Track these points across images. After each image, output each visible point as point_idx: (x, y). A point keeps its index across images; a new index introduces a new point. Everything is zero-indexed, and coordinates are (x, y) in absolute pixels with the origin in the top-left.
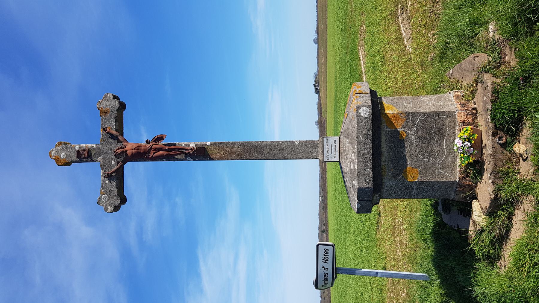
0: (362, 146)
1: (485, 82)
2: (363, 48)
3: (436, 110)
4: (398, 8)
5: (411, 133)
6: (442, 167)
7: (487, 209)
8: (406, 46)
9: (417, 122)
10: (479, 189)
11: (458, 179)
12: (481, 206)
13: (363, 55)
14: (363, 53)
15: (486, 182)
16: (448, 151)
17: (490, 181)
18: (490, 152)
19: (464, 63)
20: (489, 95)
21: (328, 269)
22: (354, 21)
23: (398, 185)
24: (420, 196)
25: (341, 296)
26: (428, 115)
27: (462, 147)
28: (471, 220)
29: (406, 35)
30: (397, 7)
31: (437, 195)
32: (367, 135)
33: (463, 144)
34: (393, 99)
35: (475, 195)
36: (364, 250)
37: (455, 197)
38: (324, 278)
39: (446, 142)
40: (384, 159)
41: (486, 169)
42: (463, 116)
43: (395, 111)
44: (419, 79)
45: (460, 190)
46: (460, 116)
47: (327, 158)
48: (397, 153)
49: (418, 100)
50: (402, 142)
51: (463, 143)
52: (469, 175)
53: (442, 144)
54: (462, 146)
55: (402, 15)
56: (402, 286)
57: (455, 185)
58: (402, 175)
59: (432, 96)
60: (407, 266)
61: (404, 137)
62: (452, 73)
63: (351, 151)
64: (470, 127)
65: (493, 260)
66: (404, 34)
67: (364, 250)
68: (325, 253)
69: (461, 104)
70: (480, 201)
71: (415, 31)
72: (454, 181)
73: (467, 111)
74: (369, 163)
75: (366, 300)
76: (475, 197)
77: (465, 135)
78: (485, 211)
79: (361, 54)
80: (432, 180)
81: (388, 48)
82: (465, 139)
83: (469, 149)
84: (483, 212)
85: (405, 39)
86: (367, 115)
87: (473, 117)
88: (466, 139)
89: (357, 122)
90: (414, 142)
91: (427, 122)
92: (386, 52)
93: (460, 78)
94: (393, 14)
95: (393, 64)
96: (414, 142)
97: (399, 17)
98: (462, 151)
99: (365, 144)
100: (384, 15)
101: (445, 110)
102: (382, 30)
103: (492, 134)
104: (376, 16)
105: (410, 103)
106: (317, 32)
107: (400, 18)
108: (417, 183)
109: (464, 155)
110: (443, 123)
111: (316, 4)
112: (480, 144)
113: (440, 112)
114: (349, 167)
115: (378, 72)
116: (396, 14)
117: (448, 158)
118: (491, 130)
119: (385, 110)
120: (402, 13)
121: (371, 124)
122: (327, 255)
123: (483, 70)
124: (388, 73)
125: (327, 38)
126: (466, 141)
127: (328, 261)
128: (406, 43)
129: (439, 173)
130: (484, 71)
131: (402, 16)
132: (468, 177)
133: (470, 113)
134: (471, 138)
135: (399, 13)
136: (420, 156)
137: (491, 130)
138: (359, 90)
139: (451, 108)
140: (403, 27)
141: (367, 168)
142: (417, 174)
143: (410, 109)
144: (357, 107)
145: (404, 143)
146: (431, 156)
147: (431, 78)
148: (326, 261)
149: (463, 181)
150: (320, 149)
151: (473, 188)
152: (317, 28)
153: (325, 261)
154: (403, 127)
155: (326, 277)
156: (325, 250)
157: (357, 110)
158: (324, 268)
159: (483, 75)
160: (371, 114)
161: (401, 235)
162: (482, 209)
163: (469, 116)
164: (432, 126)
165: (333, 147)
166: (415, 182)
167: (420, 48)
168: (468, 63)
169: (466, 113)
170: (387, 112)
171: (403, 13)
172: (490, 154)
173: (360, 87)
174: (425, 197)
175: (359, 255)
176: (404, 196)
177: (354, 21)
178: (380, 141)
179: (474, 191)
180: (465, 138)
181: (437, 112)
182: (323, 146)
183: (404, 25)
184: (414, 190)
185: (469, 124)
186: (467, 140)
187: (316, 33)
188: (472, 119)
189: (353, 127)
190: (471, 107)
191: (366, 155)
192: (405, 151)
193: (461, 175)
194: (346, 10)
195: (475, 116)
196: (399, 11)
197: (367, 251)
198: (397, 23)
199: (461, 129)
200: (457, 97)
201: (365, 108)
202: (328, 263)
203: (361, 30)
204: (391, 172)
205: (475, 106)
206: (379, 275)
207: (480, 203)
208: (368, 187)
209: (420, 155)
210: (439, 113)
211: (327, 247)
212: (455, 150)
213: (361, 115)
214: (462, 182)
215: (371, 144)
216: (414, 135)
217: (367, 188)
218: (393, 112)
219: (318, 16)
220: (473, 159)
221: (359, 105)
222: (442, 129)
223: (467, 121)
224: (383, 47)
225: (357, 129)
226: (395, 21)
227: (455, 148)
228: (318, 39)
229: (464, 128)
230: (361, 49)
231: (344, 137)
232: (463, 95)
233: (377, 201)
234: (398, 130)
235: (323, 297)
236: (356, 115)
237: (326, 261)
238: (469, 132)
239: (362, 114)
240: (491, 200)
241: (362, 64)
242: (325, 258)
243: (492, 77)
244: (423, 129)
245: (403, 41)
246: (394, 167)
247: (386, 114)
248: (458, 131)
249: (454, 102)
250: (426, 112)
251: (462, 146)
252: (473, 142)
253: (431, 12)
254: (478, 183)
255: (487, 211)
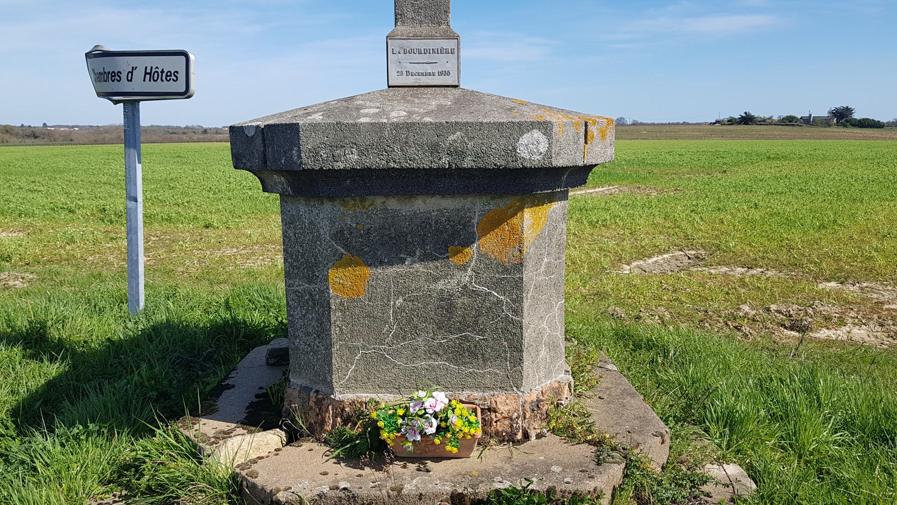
0: (430, 137)
1: (601, 469)
2: (617, 192)
3: (526, 342)
4: (700, 249)
5: (466, 277)
6: (371, 357)
7: (249, 478)
8: (628, 265)
9: (496, 294)
10: (311, 450)
11: (338, 396)
12: (262, 458)
13: (603, 192)
14: (606, 192)
15: (325, 474)
16: (414, 372)
17: (326, 489)
18: (409, 488)
19: (637, 403)
20: (568, 483)
21: (131, 80)
22: (661, 177)
23: (319, 243)
24: (293, 300)
25: (179, 156)
26: (512, 322)
27: (424, 411)
28: (233, 425)
29: (649, 264)
30: (701, 248)
31: (296, 344)
32: (462, 154)
33: (431, 415)
34: (560, 230)
35: (297, 439)
36: (250, 193)
37: (293, 385)
38: (109, 73)
39: (438, 366)
40: (393, 204)
41: (360, 476)
42: (507, 408)
43: (529, 235)
44: (570, 289)
45: (311, 402)
46: (507, 401)
47: (396, 50)
48: (409, 239)
49: (554, 295)
50: (441, 254)
51: (435, 415)
52: (350, 424)
53: (433, 356)
54: (426, 413)
55: (687, 257)
56: (162, 257)
57: (322, 388)
58: (345, 252)
59: (562, 328)
60: (198, 265)
61: (454, 260)
62: (607, 370)
63: (413, 109)
64: (479, 434)
65: (125, 482)
66: (650, 261)
67: (250, 193)
68: (169, 74)
69: (539, 401)
70: (277, 455)
71: (663, 281)
72: (333, 388)
73: (520, 419)
74: (378, 160)
75: (158, 195)
76: (293, 437)
77: (454, 420)
78: (246, 471)
79: (605, 188)
80: (334, 332)
81: (622, 233)
82: (446, 419)
83: (417, 432)
84: (242, 467)
85: (642, 262)
86: (523, 152)
87: (504, 434)
88: (446, 422)
89: (502, 124)
90: (440, 285)
91: (493, 320)
92: (615, 230)
93: (600, 391)
94: (689, 241)
95: (595, 240)
96: (440, 285)
97: (682, 251)
98: (411, 410)
99: (434, 149)
100: (684, 224)
101: (526, 363)
102: (655, 222)
103: (459, 494)
104: (679, 211)
105: (546, 273)
106: (635, 124)
107: (681, 253)
108: (324, 292)
109: (400, 416)
110: (490, 359)
111: (681, 122)
112: (430, 455)
113: (522, 351)
114: (368, 103)
115: (577, 215)
116: (687, 246)
117: (395, 371)
118: (470, 490)
119: (531, 207)
120: (690, 256)
121: (495, 165)
122: (164, 78)
123: (632, 461)
124: (576, 232)
125: (625, 139)
126: (441, 421)
127: (150, 81)
128: (635, 264)
129: (353, 350)
130: (630, 465)
131: (683, 258)
132: (345, 422)
133: (515, 425)
134: (449, 435)
135: (690, 252)
136: (401, 300)
137: (470, 490)
138: (595, 134)
139: (531, 377)
140: (664, 259)
141: (361, 153)
142: (350, 293)
143: (531, 276)
144: (550, 122)
145: (437, 259)
146: (401, 329)
147: (574, 311)
148: (148, 76)
149: (333, 410)
150: (424, 29)
151: (314, 432)
152: (641, 124)
153: (149, 74)
154: (482, 256)
155: (112, 76)
156: (176, 74)
157: (539, 123)
158: (131, 70)
159: (619, 463)
160: (525, 164)
161: (265, 256)
162: (254, 462)
163: (507, 422)
164: (482, 332)
165: (429, 69)
166: (328, 288)
167: (631, 291)
168: (641, 415)
169: (516, 415)
170: (528, 213)
171: (689, 258)
172: (402, 489)
173: (603, 137)
174: (291, 313)
175: (242, 185)
176: (292, 258)
177: (661, 177)
178: (445, 193)
179: (308, 437)
180: (450, 421)
181: (521, 344)
182: (432, 37)
183: (668, 261)
184: (307, 285)
185: (486, 423)
186: (443, 424)
187: (634, 121)
188: (500, 430)
189: (486, 113)
190: (531, 427)
191: (402, 150)
192: (413, 262)
193: (350, 404)
194: (680, 165)
195: (507, 438)
196: (693, 252)
197: (248, 198)
198: (671, 247)
199: (473, 403)
200: (557, 392)
201: (543, 147)
202: (144, 80)
203: (648, 189)
204: (354, 225)
205: (533, 438)
206: (131, 204)
207: (271, 455)
208: (303, 155)
209: (404, 300)
210: (518, 348)
211: (182, 76)
212: (417, 393)
213: (525, 136)
214: (330, 407)
215: (434, 166)
216: (458, 285)
217: (299, 151)
218: (525, 229)
219: (662, 124)
220: (389, 441)
221: (555, 129)
222: (476, 356)
223: (495, 420)
224: (623, 224)
225: (481, 123)
226: (675, 245)
227: (421, 394)
228: (624, 125)
229: (476, 416)
230: (614, 189)
231: (457, 96)
232: (561, 404)
233: (271, 186)
234: (474, 242)
235: (186, 131)
236: (523, 120)
237: (148, 76)
238: (466, 430)
239: (525, 139)
240: (271, 491)
241: (588, 191)
242: (156, 74)
243: (614, 486)
244: (475, 309)
245: (637, 259)
246: (368, 232)
247: (521, 209)
248: (469, 396)
249: (544, 384)
250: (522, 316)
251: (426, 413)
252: (437, 441)
253: (706, 312)
254: (328, 448)
255: (244, 477)
